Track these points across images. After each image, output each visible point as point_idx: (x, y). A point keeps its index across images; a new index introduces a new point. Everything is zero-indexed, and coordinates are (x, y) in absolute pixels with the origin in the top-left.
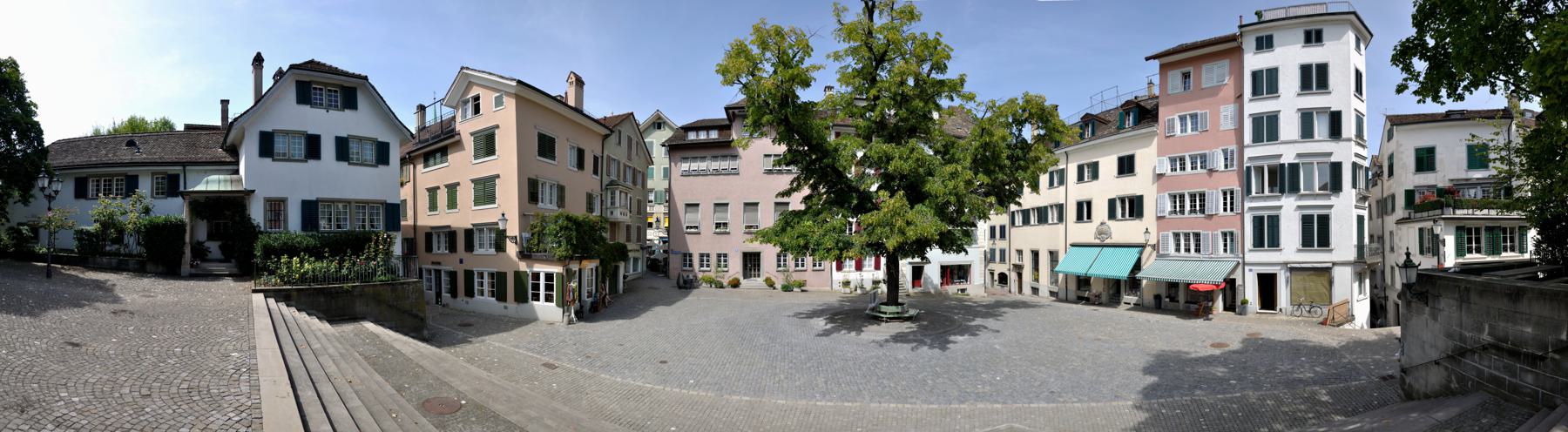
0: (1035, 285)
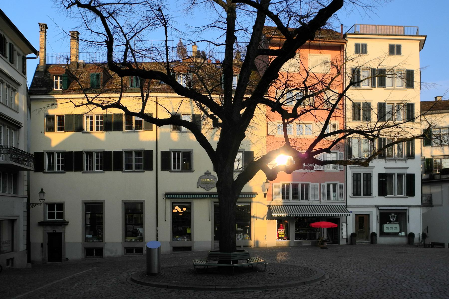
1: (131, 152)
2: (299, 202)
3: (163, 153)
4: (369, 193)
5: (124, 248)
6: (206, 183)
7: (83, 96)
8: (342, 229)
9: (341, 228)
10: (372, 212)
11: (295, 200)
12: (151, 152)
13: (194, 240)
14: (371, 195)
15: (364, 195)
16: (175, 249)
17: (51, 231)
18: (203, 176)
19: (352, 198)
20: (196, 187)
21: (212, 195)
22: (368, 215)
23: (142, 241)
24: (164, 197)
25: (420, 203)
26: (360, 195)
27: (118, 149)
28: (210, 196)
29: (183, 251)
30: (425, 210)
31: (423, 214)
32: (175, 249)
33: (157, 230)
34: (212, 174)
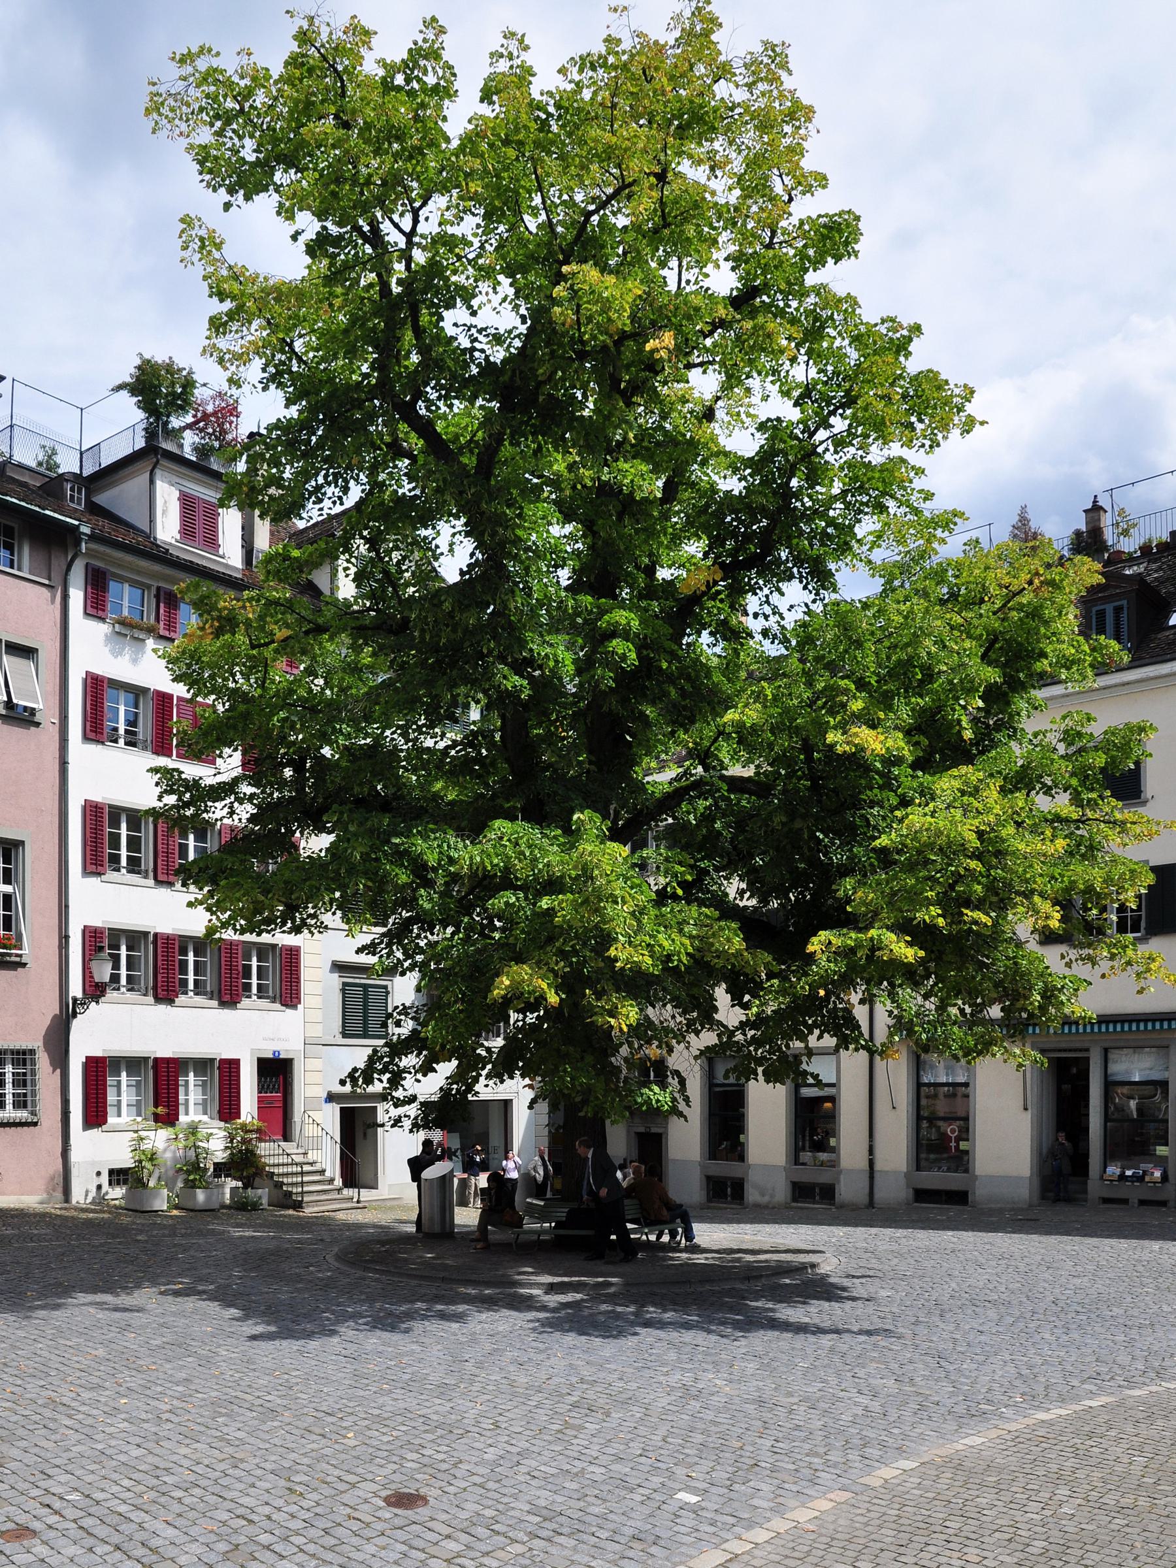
0: (725, 1168)
13: (978, 1172)
17: (642, 1130)
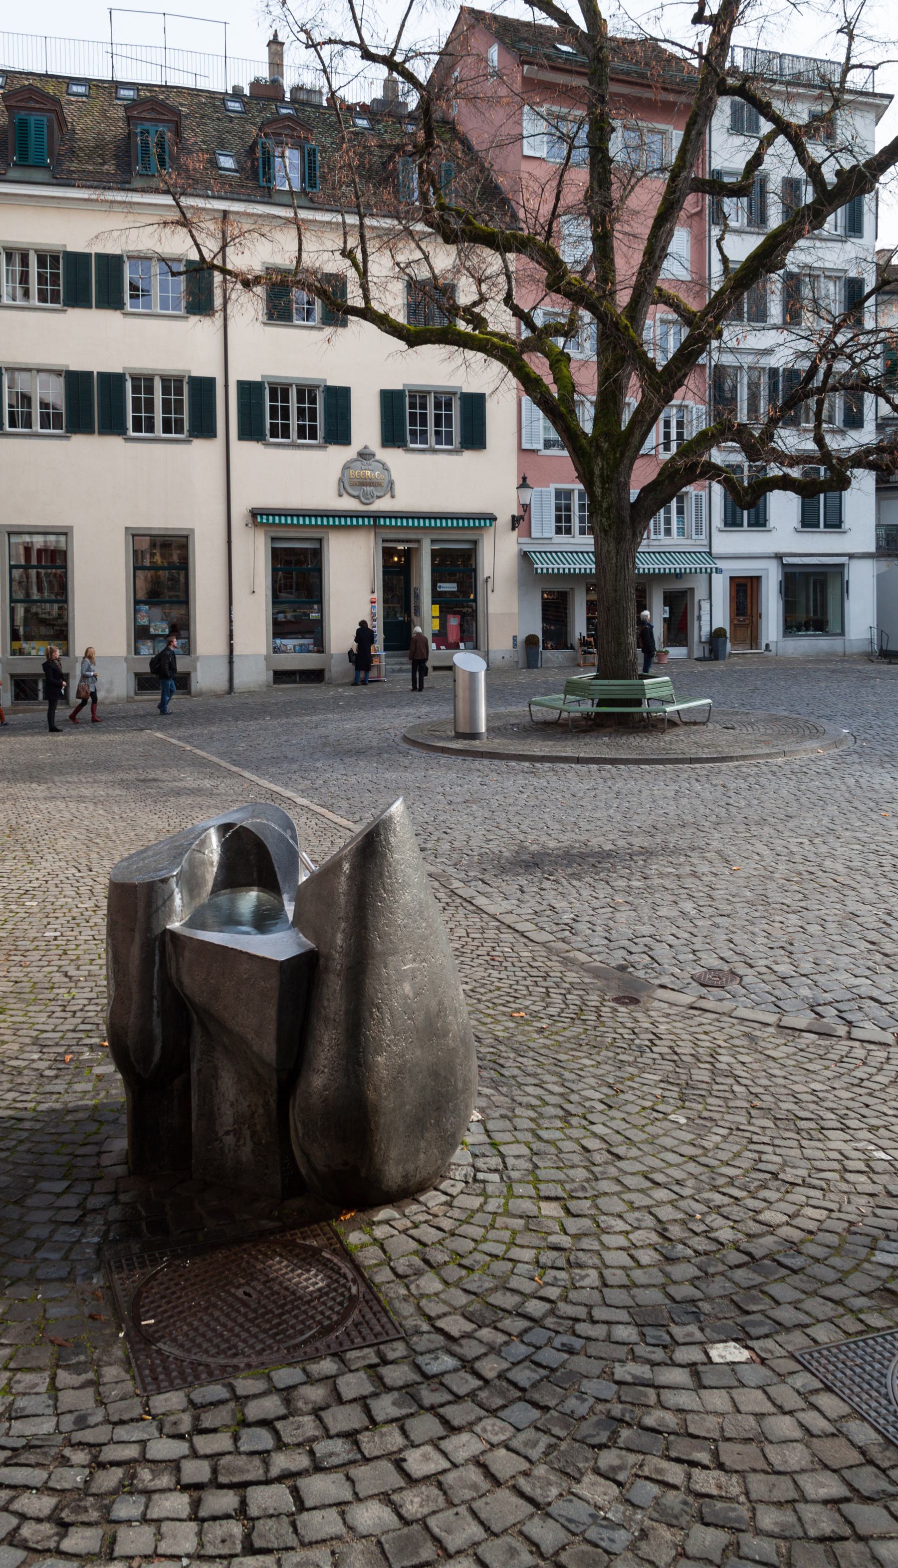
1: (149, 380)
2: (572, 541)
3: (241, 384)
4: (762, 522)
5: (133, 676)
6: (364, 483)
7: (168, 200)
8: (699, 618)
9: (696, 614)
10: (767, 570)
11: (563, 538)
12: (211, 381)
14: (764, 525)
15: (749, 525)
16: (281, 676)
18: (356, 460)
19: (723, 534)
20: (336, 493)
21: (379, 517)
22: (758, 578)
23: (189, 654)
24: (250, 520)
25: (872, 549)
26: (741, 525)
27: (115, 368)
28: (375, 521)
29: (302, 681)
30: (884, 565)
31: (878, 576)
32: (281, 676)
33: (231, 621)
34: (378, 457)
